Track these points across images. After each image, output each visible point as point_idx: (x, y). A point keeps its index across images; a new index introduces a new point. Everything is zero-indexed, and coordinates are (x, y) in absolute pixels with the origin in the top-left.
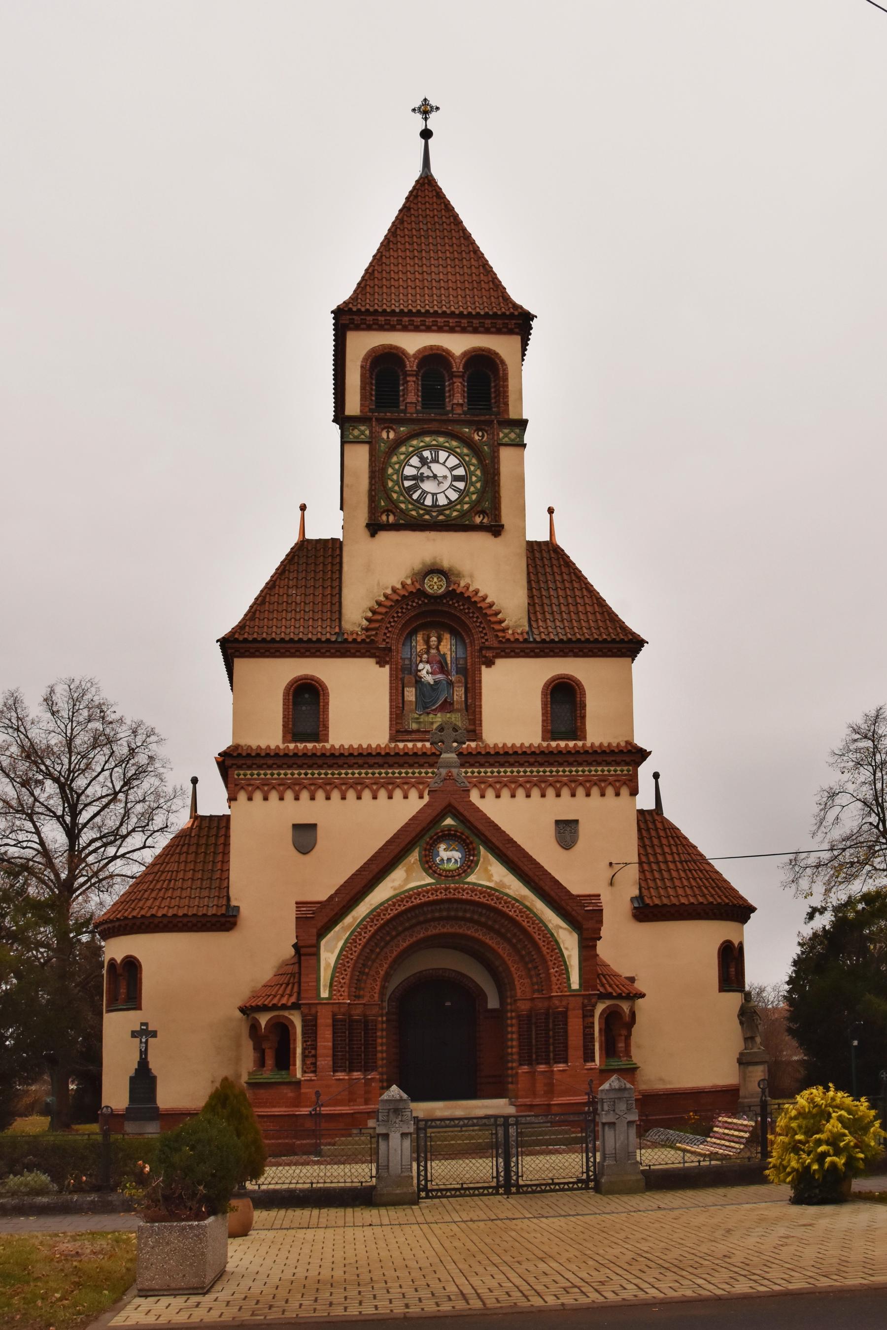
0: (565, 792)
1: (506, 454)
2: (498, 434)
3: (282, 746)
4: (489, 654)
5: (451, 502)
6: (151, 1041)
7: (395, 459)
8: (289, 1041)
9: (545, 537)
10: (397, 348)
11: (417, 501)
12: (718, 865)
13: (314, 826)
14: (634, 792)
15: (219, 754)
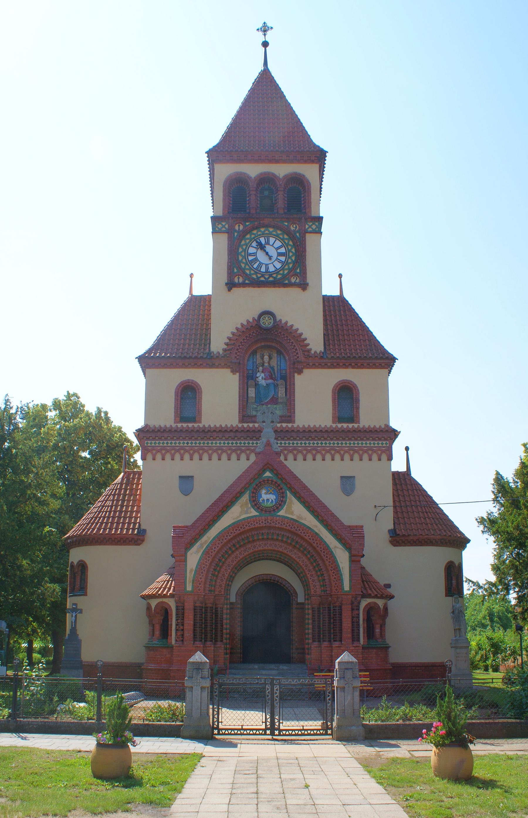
0: (347, 457)
1: (309, 238)
3: (174, 425)
6: (79, 615)
7: (243, 242)
12: (447, 510)
13: (192, 477)
15: (136, 430)
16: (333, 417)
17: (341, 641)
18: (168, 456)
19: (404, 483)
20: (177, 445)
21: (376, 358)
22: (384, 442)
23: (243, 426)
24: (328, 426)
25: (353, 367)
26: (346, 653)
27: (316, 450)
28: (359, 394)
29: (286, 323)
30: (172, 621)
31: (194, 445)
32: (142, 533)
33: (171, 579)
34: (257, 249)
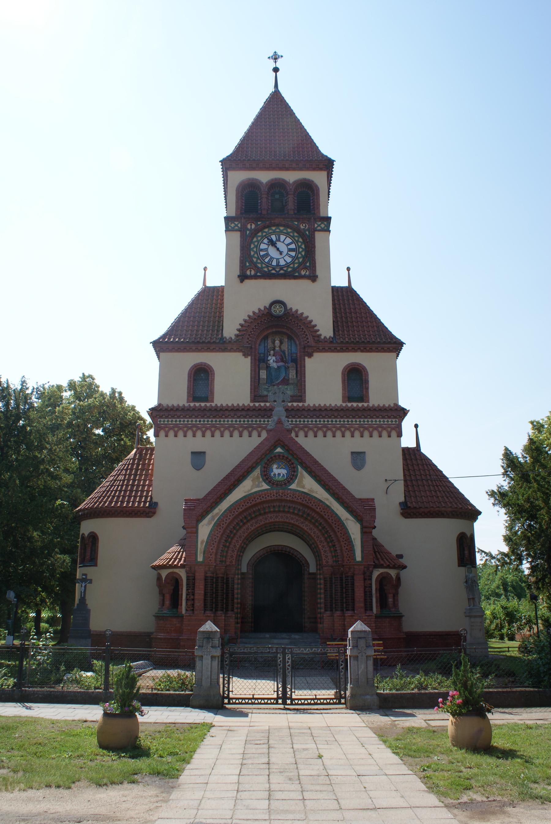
1: (319, 236)
2: (314, 225)
4: (310, 350)
7: (255, 239)
9: (344, 283)
10: (309, 180)
11: (268, 263)
13: (204, 453)
14: (400, 435)
17: (353, 610)
21: (385, 343)
23: (254, 405)
24: (339, 405)
25: (362, 351)
26: (359, 622)
28: (368, 375)
29: (297, 311)
30: (182, 591)
31: (206, 422)
34: (268, 245)
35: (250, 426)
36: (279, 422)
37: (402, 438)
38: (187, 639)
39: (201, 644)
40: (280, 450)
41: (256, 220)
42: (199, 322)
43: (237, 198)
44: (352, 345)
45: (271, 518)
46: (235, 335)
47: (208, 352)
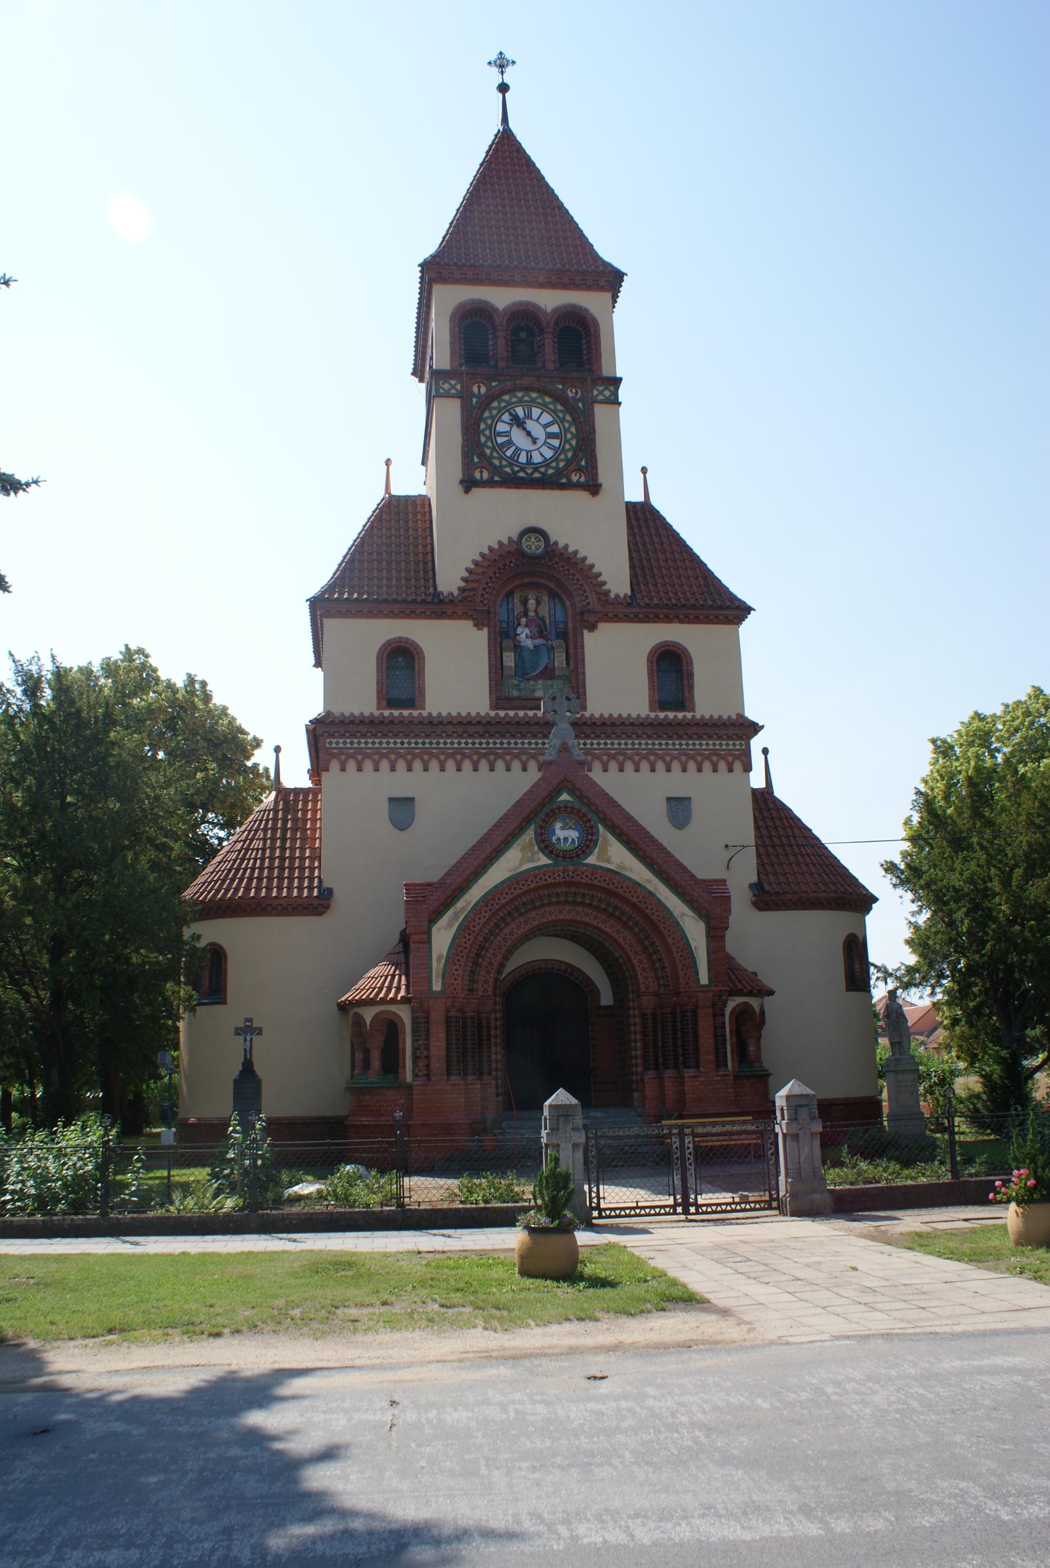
0: (676, 766)
1: (600, 411)
3: (377, 713)
5: (546, 460)
6: (256, 1038)
7: (487, 414)
8: (398, 1039)
9: (640, 498)
10: (580, 308)
11: (512, 457)
12: (834, 850)
13: (412, 799)
14: (748, 768)
16: (651, 702)
17: (697, 1067)
18: (368, 765)
19: (766, 804)
20: (384, 745)
21: (711, 607)
22: (738, 743)
23: (497, 714)
24: (643, 716)
25: (681, 622)
26: (561, 1090)
27: (624, 755)
29: (566, 547)
30: (404, 1043)
31: (413, 745)
32: (327, 894)
33: (397, 972)
34: (511, 425)
35: (491, 751)
36: (564, 748)
37: (751, 773)
38: (422, 1125)
39: (555, 1126)
40: (567, 800)
41: (487, 379)
42: (389, 563)
43: (452, 336)
44: (665, 611)
45: (551, 913)
46: (459, 589)
47: (402, 618)
